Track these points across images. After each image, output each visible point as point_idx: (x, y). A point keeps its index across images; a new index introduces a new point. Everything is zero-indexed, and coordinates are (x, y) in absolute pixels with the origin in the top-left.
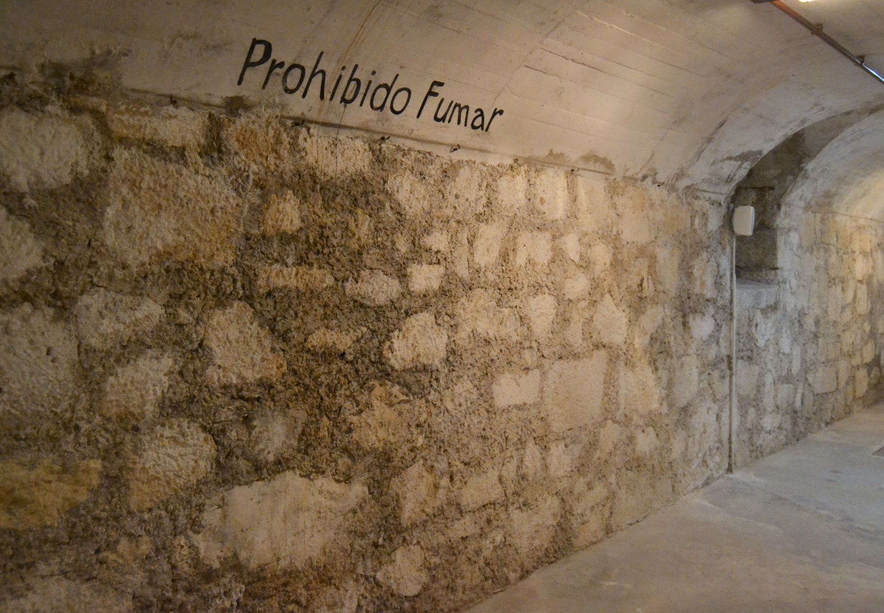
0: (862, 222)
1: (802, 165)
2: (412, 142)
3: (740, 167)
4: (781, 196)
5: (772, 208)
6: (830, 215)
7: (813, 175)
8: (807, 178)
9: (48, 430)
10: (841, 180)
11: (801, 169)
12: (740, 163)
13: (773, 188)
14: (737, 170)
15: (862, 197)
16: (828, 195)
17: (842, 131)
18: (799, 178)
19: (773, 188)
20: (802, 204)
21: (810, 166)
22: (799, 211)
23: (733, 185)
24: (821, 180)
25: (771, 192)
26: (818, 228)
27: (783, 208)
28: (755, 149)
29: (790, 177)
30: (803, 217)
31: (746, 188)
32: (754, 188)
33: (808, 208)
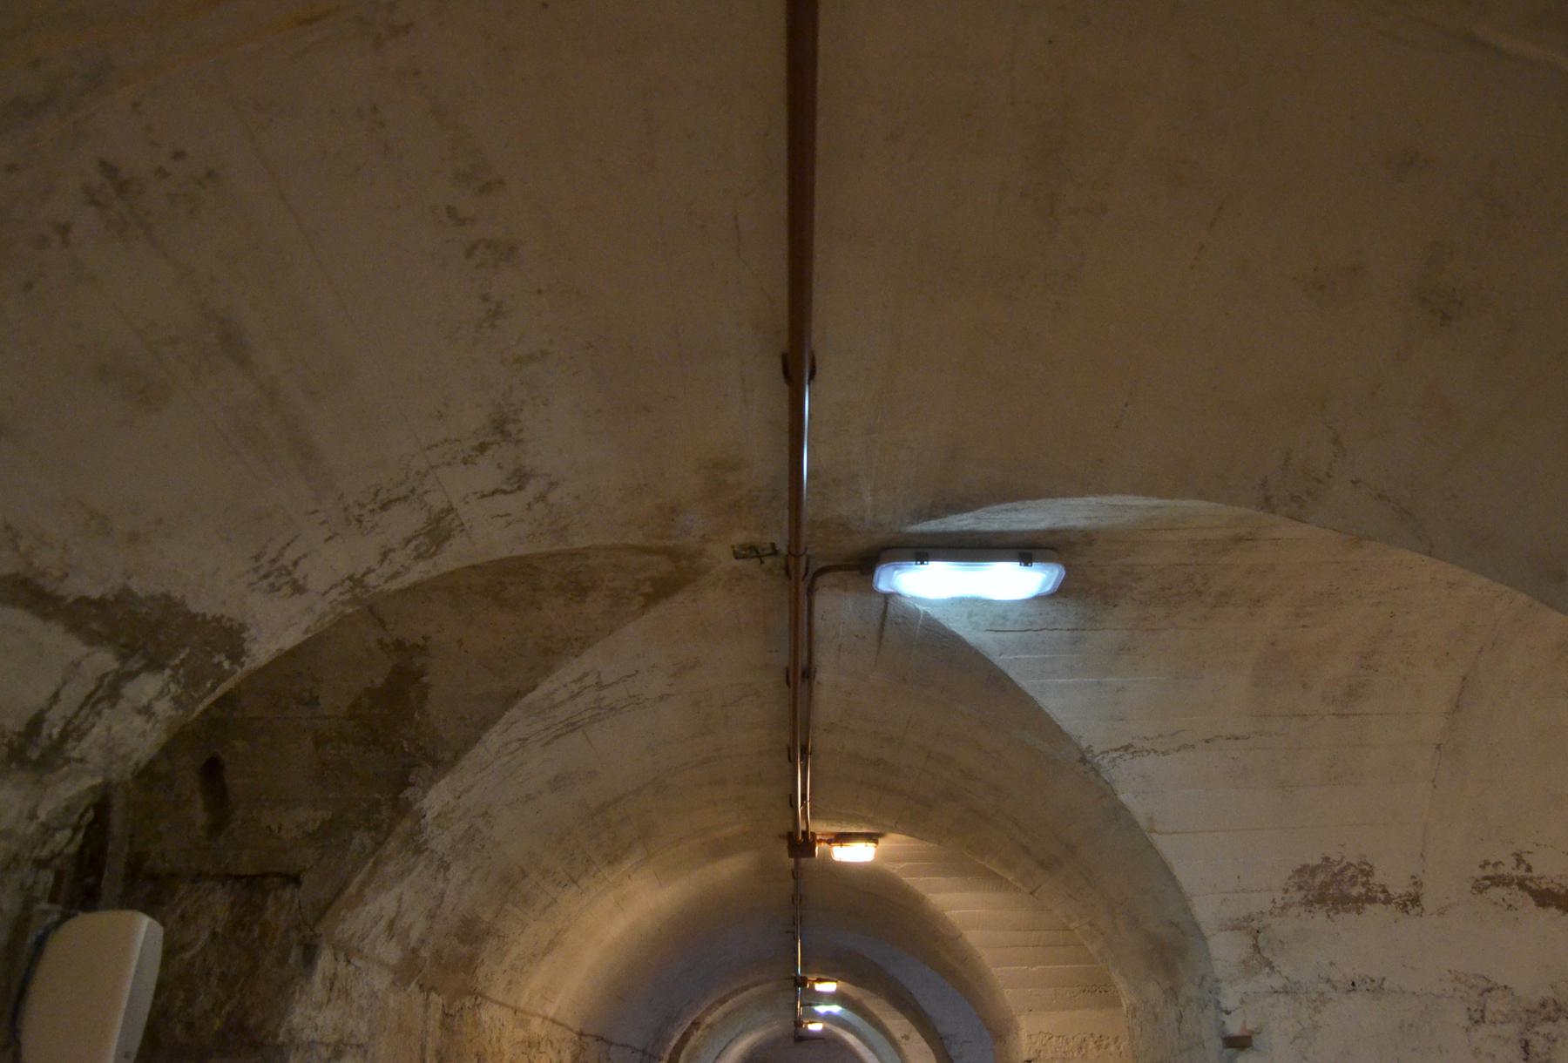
0: (537, 1027)
1: (408, 792)
2: (880, 1037)
3: (109, 691)
4: (323, 909)
5: (282, 961)
6: (468, 1002)
7: (440, 842)
8: (418, 850)
9: (380, 642)
10: (512, 886)
11: (402, 809)
12: (105, 660)
13: (296, 880)
14: (91, 702)
15: (545, 954)
16: (473, 935)
17: (549, 670)
18: (392, 844)
19: (296, 880)
20: (391, 953)
21: (436, 799)
22: (380, 981)
23: (68, 790)
24: (457, 873)
25: (287, 894)
26: (431, 1047)
27: (325, 962)
28: (204, 605)
29: (361, 838)
30: (392, 1001)
31: (199, 876)
32: (225, 878)
33: (408, 971)
